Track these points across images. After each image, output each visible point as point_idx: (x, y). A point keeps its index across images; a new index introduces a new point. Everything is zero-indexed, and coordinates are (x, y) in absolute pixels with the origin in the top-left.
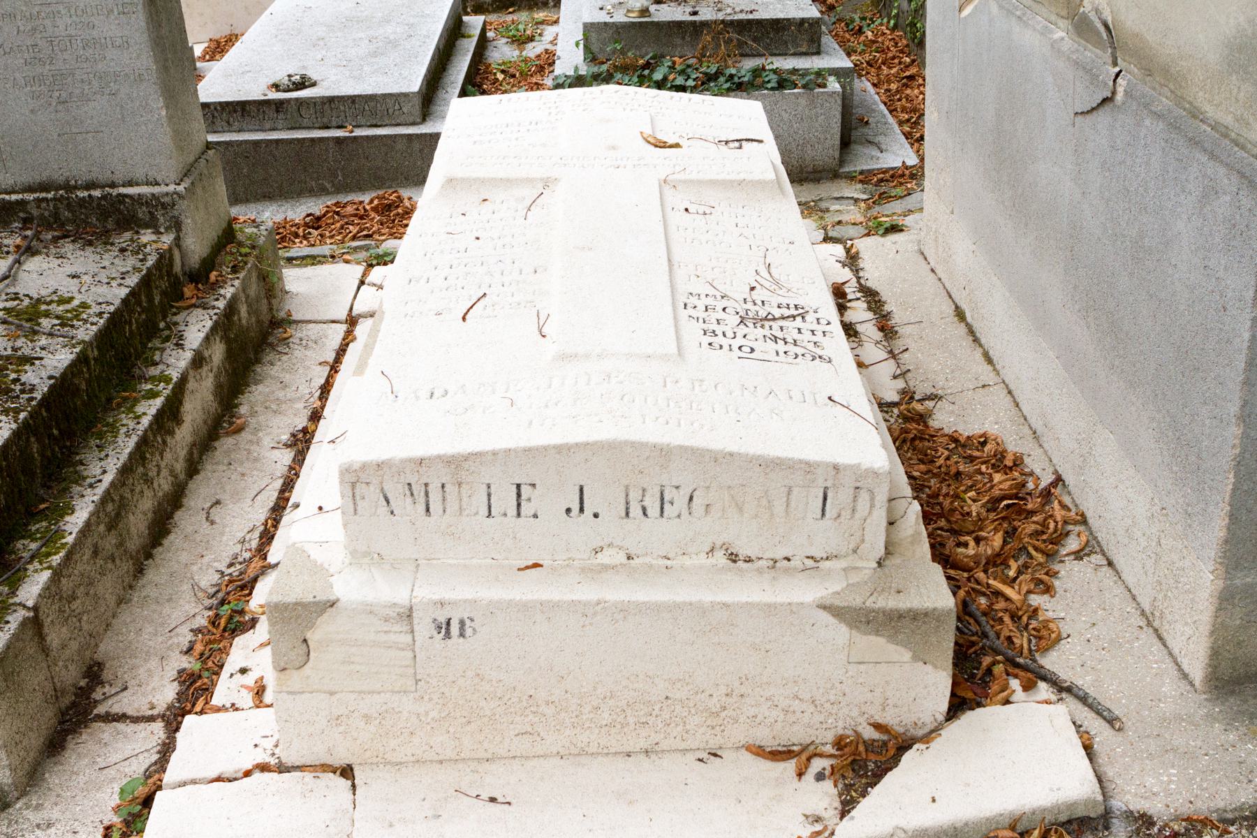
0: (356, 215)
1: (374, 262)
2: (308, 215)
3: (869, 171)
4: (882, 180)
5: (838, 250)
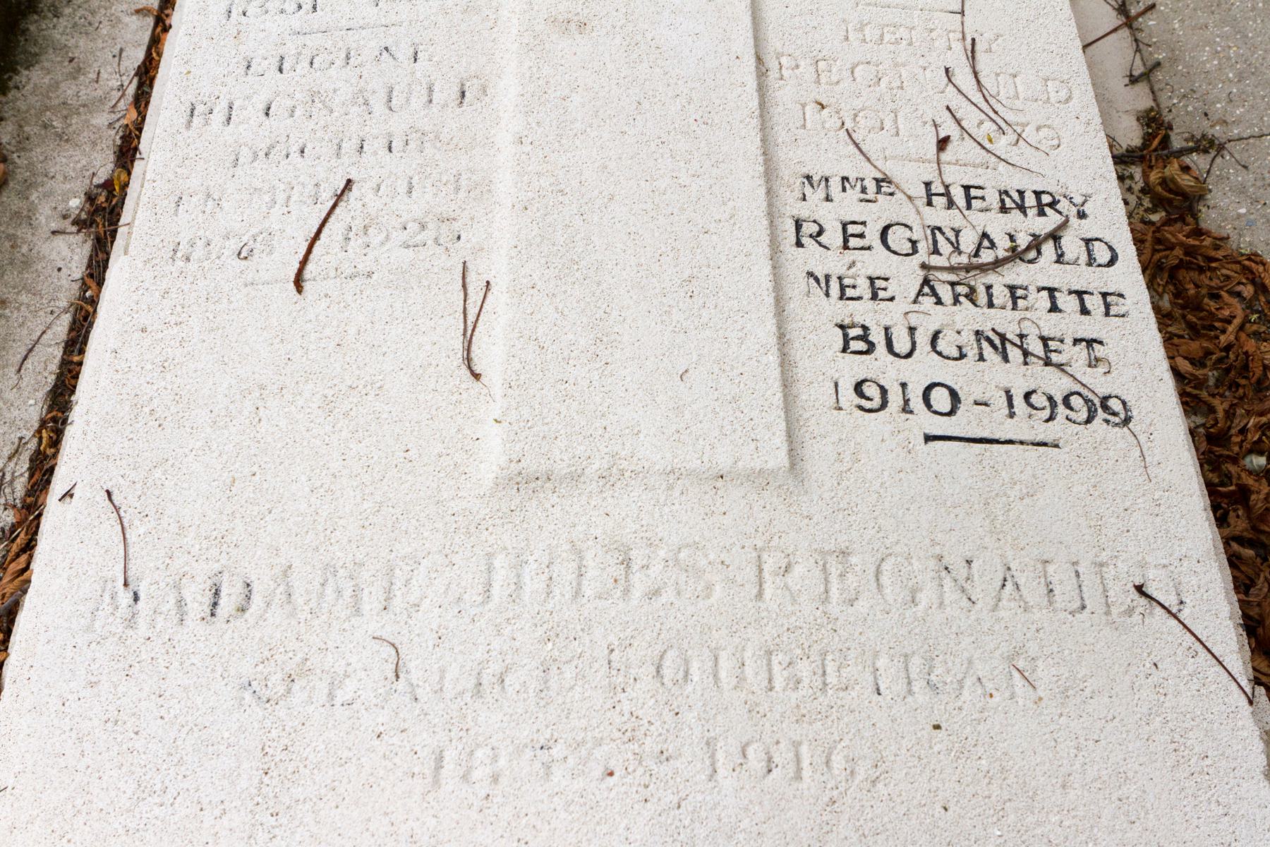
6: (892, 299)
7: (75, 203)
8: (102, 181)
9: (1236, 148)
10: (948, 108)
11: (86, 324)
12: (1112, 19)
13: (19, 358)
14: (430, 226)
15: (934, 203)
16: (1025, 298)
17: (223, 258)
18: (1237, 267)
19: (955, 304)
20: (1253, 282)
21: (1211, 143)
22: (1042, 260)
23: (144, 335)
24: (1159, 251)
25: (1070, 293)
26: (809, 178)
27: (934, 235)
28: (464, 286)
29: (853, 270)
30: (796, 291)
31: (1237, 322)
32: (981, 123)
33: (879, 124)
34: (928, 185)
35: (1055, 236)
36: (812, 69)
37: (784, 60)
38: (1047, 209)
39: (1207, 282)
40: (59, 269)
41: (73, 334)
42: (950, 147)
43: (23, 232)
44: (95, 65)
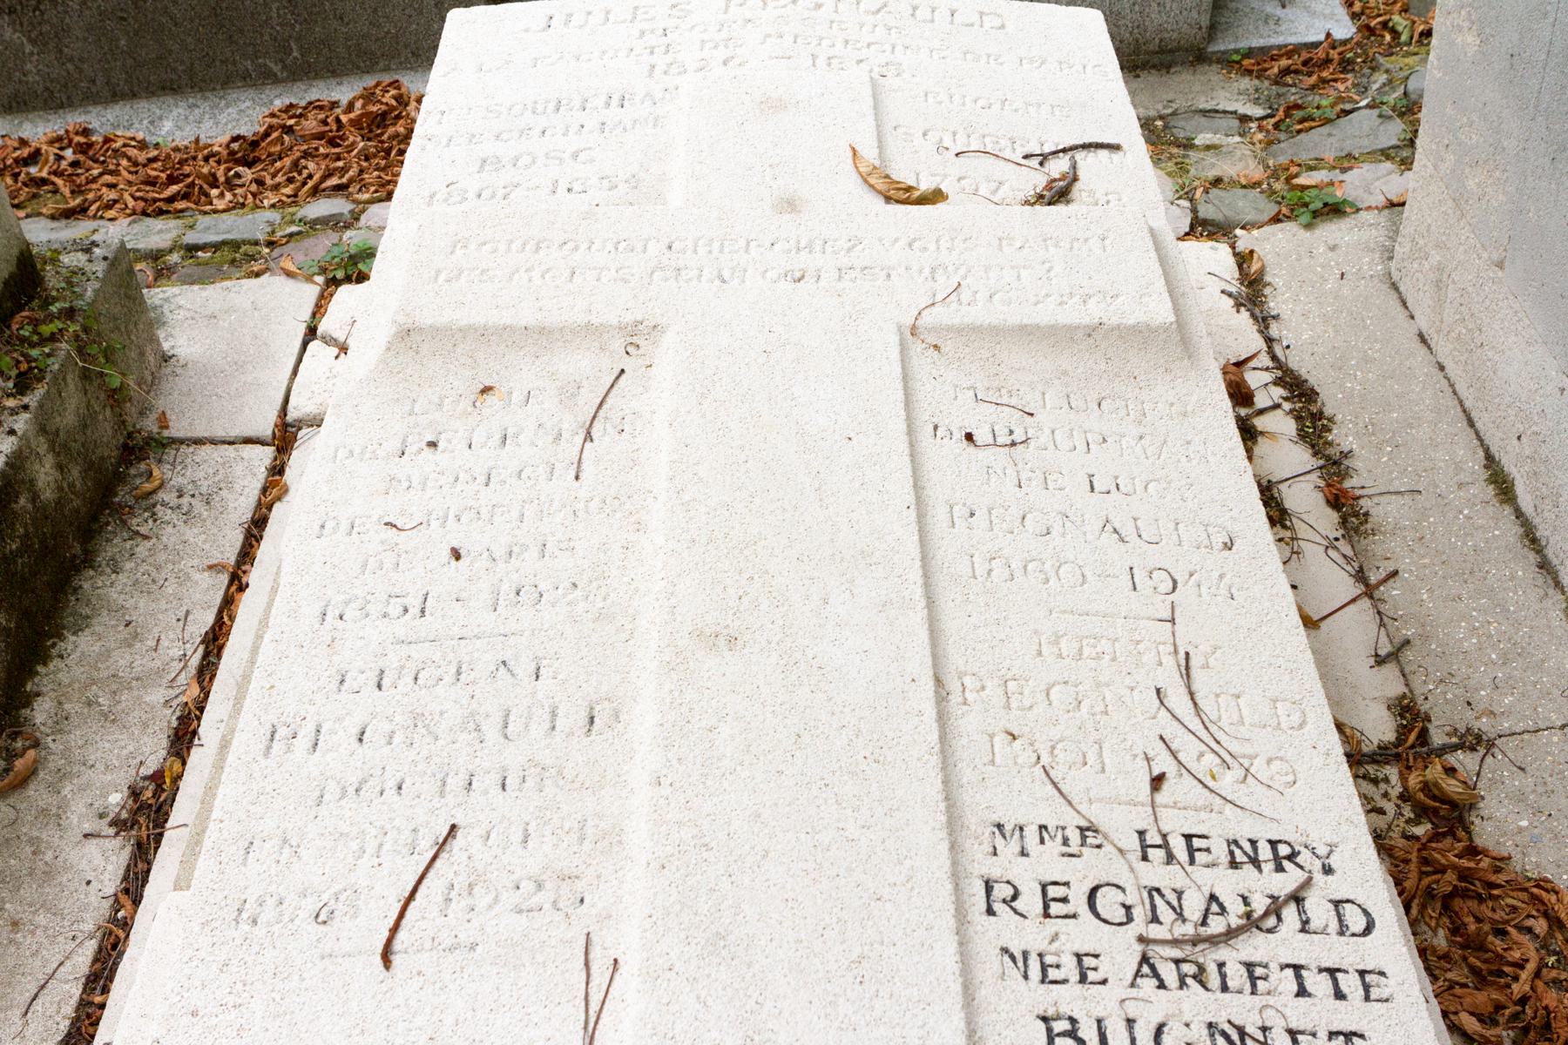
0: (320, 136)
1: (340, 274)
2: (235, 139)
3: (1262, 49)
4: (1286, 71)
5: (1215, 258)
6: (1104, 982)
7: (116, 798)
8: (150, 772)
9: (1508, 745)
10: (1161, 738)
11: (114, 954)
12: (1351, 588)
13: (28, 996)
14: (548, 885)
15: (1150, 857)
16: (1265, 979)
17: (297, 922)
18: (1524, 896)
19: (1181, 988)
20: (1546, 915)
21: (1479, 738)
22: (1283, 928)
23: (195, 1020)
24: (1427, 874)
25: (1321, 970)
26: (999, 826)
27: (1151, 897)
28: (587, 964)
29: (1056, 945)
30: (988, 973)
31: (1531, 966)
32: (1202, 755)
33: (1080, 758)
34: (1141, 833)
35: (1297, 898)
36: (1000, 691)
37: (967, 680)
38: (1286, 863)
39: (1490, 914)
40: (89, 883)
41: (98, 965)
42: (1166, 786)
43: (48, 834)
44: (156, 630)
